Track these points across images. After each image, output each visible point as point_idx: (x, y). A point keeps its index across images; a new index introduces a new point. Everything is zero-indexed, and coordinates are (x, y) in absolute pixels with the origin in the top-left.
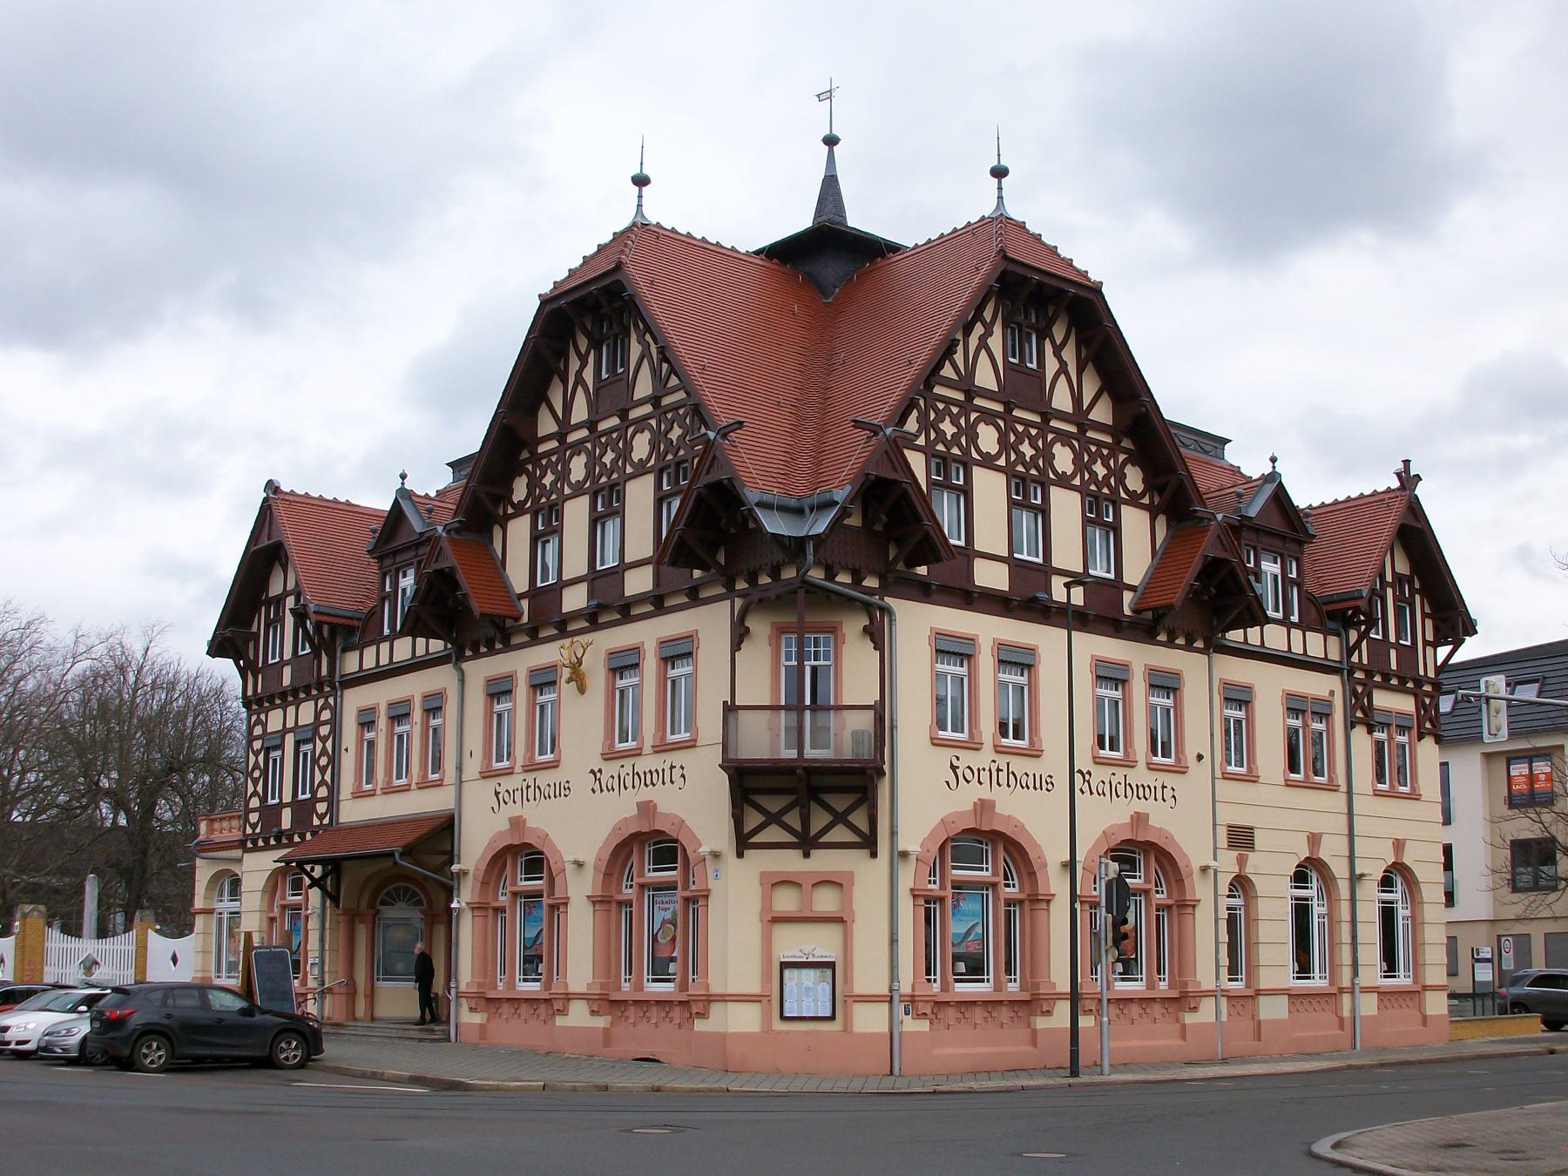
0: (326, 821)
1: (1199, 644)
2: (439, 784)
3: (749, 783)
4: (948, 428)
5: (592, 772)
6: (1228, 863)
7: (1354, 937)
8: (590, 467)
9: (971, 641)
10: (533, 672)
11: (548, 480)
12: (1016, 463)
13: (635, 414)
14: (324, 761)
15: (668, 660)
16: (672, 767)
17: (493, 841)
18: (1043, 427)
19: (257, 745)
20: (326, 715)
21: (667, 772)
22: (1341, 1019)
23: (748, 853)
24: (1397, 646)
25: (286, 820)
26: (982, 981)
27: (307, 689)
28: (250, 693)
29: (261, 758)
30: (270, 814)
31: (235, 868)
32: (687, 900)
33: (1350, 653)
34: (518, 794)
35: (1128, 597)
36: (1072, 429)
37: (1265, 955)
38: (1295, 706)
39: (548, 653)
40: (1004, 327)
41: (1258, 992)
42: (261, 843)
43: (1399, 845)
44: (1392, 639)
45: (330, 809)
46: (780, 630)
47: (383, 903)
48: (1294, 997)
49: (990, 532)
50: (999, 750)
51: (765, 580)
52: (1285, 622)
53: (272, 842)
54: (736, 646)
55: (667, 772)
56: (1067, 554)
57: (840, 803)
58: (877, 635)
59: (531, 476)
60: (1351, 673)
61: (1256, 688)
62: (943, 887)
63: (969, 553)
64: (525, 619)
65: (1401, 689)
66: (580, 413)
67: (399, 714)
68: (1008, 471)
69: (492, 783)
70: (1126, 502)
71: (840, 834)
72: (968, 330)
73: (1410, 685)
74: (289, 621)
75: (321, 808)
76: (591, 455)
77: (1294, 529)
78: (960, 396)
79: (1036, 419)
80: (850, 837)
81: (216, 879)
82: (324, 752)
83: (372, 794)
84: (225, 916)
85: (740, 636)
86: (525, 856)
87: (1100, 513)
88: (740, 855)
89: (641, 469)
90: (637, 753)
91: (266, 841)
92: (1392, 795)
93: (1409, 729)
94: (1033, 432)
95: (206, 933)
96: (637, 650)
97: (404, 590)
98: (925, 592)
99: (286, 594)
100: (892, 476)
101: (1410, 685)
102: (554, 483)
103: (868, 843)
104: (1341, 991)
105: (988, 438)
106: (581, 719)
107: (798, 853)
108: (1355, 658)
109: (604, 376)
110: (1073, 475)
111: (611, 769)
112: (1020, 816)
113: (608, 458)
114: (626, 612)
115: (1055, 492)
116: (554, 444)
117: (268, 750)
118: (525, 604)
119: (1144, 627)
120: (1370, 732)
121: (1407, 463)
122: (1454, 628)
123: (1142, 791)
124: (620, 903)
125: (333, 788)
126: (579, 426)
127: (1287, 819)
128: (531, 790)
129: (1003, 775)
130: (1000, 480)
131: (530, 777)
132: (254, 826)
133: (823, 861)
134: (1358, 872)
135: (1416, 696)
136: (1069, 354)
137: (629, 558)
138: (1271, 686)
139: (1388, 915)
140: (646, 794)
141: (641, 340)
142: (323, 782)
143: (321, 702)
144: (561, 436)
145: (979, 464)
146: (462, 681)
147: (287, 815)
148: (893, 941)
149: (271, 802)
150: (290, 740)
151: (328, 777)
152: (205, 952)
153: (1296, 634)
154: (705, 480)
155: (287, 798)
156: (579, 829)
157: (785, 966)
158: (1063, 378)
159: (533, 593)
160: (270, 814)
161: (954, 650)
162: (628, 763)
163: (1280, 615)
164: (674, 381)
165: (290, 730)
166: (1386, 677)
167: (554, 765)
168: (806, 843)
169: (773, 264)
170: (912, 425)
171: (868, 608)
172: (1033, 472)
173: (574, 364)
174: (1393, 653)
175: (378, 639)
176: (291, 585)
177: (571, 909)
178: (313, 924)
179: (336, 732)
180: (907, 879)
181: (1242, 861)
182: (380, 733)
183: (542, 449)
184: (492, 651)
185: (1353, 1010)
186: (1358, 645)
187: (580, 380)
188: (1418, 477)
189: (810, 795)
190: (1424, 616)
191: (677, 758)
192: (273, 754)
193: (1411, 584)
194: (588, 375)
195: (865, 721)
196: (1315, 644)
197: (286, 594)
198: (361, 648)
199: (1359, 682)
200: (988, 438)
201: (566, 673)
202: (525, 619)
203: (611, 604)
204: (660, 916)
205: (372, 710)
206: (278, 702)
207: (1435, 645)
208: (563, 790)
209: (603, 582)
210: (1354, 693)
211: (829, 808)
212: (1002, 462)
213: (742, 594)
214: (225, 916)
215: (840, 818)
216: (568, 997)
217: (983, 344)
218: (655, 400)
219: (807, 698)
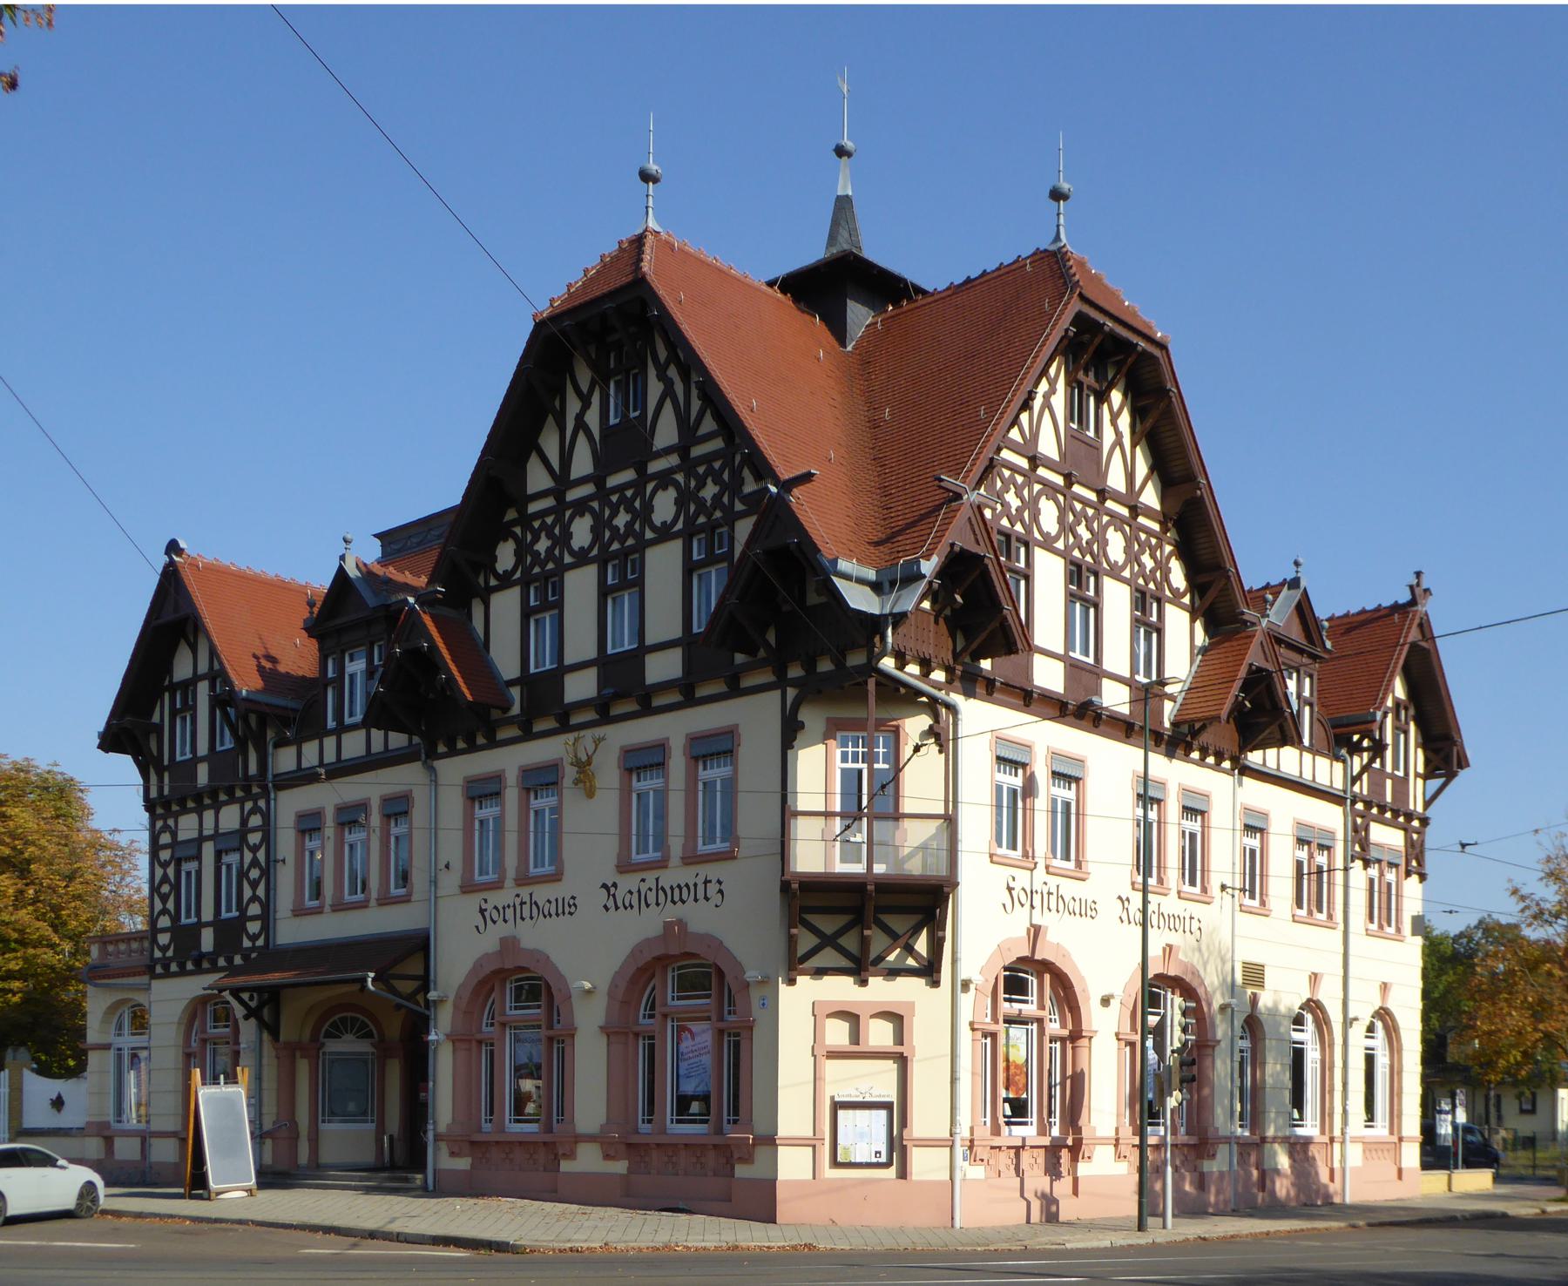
0: (260, 942)
1: (1227, 764)
2: (406, 899)
5: (604, 886)
8: (596, 531)
13: (654, 467)
14: (254, 874)
16: (706, 882)
17: (478, 964)
18: (1099, 506)
19: (165, 855)
20: (256, 820)
21: (701, 888)
25: (207, 940)
26: (1025, 1124)
27: (230, 792)
28: (154, 794)
29: (171, 871)
31: (140, 998)
32: (550, 1039)
34: (510, 912)
35: (1168, 707)
40: (1068, 383)
42: (174, 967)
43: (1385, 987)
44: (1389, 769)
45: (266, 928)
47: (328, 1035)
53: (190, 966)
55: (701, 888)
56: (1117, 657)
58: (939, 736)
59: (519, 542)
60: (1354, 803)
61: (1089, 763)
64: (516, 710)
65: (1392, 824)
67: (350, 817)
73: (1401, 819)
75: (253, 927)
76: (597, 517)
82: (255, 863)
83: (318, 911)
84: (126, 1053)
86: (524, 985)
89: (664, 534)
90: (662, 864)
91: (182, 966)
93: (1397, 866)
97: (352, 676)
99: (196, 678)
100: (974, 548)
101: (1401, 819)
105: (1049, 515)
106: (591, 826)
107: (849, 980)
108: (1356, 788)
109: (613, 421)
111: (629, 882)
112: (1066, 944)
114: (647, 703)
116: (549, 502)
117: (178, 862)
118: (515, 692)
121: (1418, 574)
122: (1447, 760)
124: (480, 1042)
128: (526, 908)
130: (1059, 564)
131: (525, 892)
133: (880, 990)
134: (1351, 1015)
135: (1405, 830)
136: (1125, 421)
137: (650, 639)
138: (1287, 812)
139: (1370, 1060)
141: (662, 376)
142: (255, 898)
143: (249, 805)
144: (558, 492)
148: (954, 1080)
150: (208, 849)
151: (261, 891)
153: (1307, 756)
156: (589, 952)
157: (837, 1106)
159: (525, 680)
162: (650, 877)
165: (209, 838)
167: (556, 877)
168: (860, 969)
169: (786, 300)
171: (933, 706)
173: (573, 406)
174: (1389, 783)
175: (320, 733)
176: (203, 667)
177: (579, 1041)
179: (268, 839)
183: (533, 508)
184: (473, 748)
187: (581, 424)
190: (1417, 746)
191: (712, 871)
192: (185, 867)
193: (1406, 709)
194: (592, 418)
196: (1327, 772)
197: (196, 678)
198: (298, 741)
200: (1049, 515)
202: (516, 710)
206: (191, 804)
208: (568, 907)
213: (794, 683)
214: (126, 1053)
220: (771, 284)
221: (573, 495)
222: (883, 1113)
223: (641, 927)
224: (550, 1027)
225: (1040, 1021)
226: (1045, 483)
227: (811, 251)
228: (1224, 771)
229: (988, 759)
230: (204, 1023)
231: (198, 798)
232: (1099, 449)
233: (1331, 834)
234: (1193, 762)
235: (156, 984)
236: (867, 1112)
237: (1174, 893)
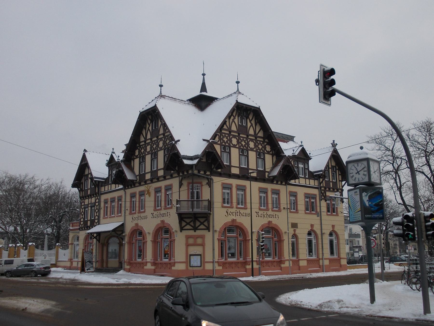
1: (284, 183)
3: (182, 217)
4: (225, 139)
6: (291, 231)
7: (322, 247)
8: (151, 148)
9: (231, 185)
10: (140, 192)
11: (143, 151)
12: (241, 146)
14: (97, 211)
15: (166, 190)
17: (132, 228)
19: (83, 207)
20: (97, 201)
22: (320, 266)
23: (183, 231)
24: (332, 182)
27: (93, 195)
30: (85, 222)
31: (78, 234)
33: (320, 184)
35: (267, 174)
36: (254, 138)
37: (300, 251)
38: (307, 196)
39: (142, 188)
40: (238, 117)
41: (341, 258)
44: (331, 180)
46: (189, 184)
48: (308, 261)
49: (235, 161)
50: (237, 208)
51: (185, 173)
52: (305, 178)
54: (180, 187)
56: (252, 165)
57: (202, 220)
58: (210, 184)
59: (139, 150)
60: (321, 188)
62: (225, 238)
63: (230, 166)
64: (138, 181)
66: (149, 136)
68: (239, 148)
69: (132, 215)
70: (266, 153)
71: (202, 227)
72: (230, 118)
74: (89, 180)
76: (151, 145)
77: (307, 157)
78: (228, 132)
79: (245, 136)
80: (204, 227)
81: (73, 237)
82: (97, 209)
85: (181, 185)
86: (138, 232)
87: (260, 155)
88: (181, 232)
90: (161, 209)
92: (331, 215)
94: (245, 139)
95: (71, 249)
96: (160, 188)
98: (220, 175)
102: (144, 151)
103: (208, 229)
104: (320, 259)
105: (234, 141)
108: (322, 185)
110: (254, 148)
111: (155, 213)
113: (155, 146)
114: (158, 180)
115: (250, 152)
116: (143, 143)
117: (85, 208)
119: (272, 180)
120: (326, 201)
121: (334, 141)
123: (270, 216)
125: (99, 217)
126: (149, 139)
127: (305, 221)
129: (238, 213)
131: (139, 214)
132: (82, 225)
133: (198, 233)
134: (323, 232)
136: (253, 122)
139: (331, 242)
140: (162, 219)
141: (161, 121)
142: (97, 215)
144: (145, 141)
145: (232, 147)
146: (125, 194)
147: (89, 222)
148: (213, 250)
149: (86, 220)
151: (98, 214)
152: (71, 253)
153: (307, 180)
154: (172, 152)
155: (89, 219)
157: (190, 255)
158: (252, 127)
160: (85, 222)
161: (225, 187)
162: (159, 212)
163: (303, 176)
164: (167, 131)
166: (329, 189)
167: (144, 212)
168: (195, 229)
170: (217, 139)
172: (245, 148)
173: (148, 126)
174: (331, 184)
178: (94, 247)
179: (99, 205)
180: (216, 236)
181: (295, 231)
182: (109, 205)
183: (141, 144)
184: (132, 187)
185: (323, 263)
186: (322, 181)
187: (149, 129)
188: (337, 144)
189: (196, 219)
190: (339, 175)
191: (168, 211)
193: (336, 168)
194: (150, 128)
195: (206, 203)
199: (323, 190)
200: (234, 141)
201: (146, 192)
202: (138, 181)
203: (155, 178)
204: (166, 244)
205: (107, 199)
207: (342, 181)
208: (146, 217)
209: (154, 173)
210: (322, 192)
211: (199, 221)
212: (238, 146)
213: (181, 176)
215: (202, 223)
216: (147, 262)
217: (233, 121)
218: (164, 134)
219: (195, 198)
220: (187, 100)
221: (147, 142)
222: (200, 257)
223: (157, 222)
224: (171, 238)
225: (237, 237)
226: (233, 136)
227: (197, 93)
228: (283, 185)
229: (220, 188)
230: (136, 235)
231: (88, 196)
232: (247, 128)
233: (316, 195)
234: (275, 184)
235: (80, 232)
236: (196, 256)
237: (270, 210)
